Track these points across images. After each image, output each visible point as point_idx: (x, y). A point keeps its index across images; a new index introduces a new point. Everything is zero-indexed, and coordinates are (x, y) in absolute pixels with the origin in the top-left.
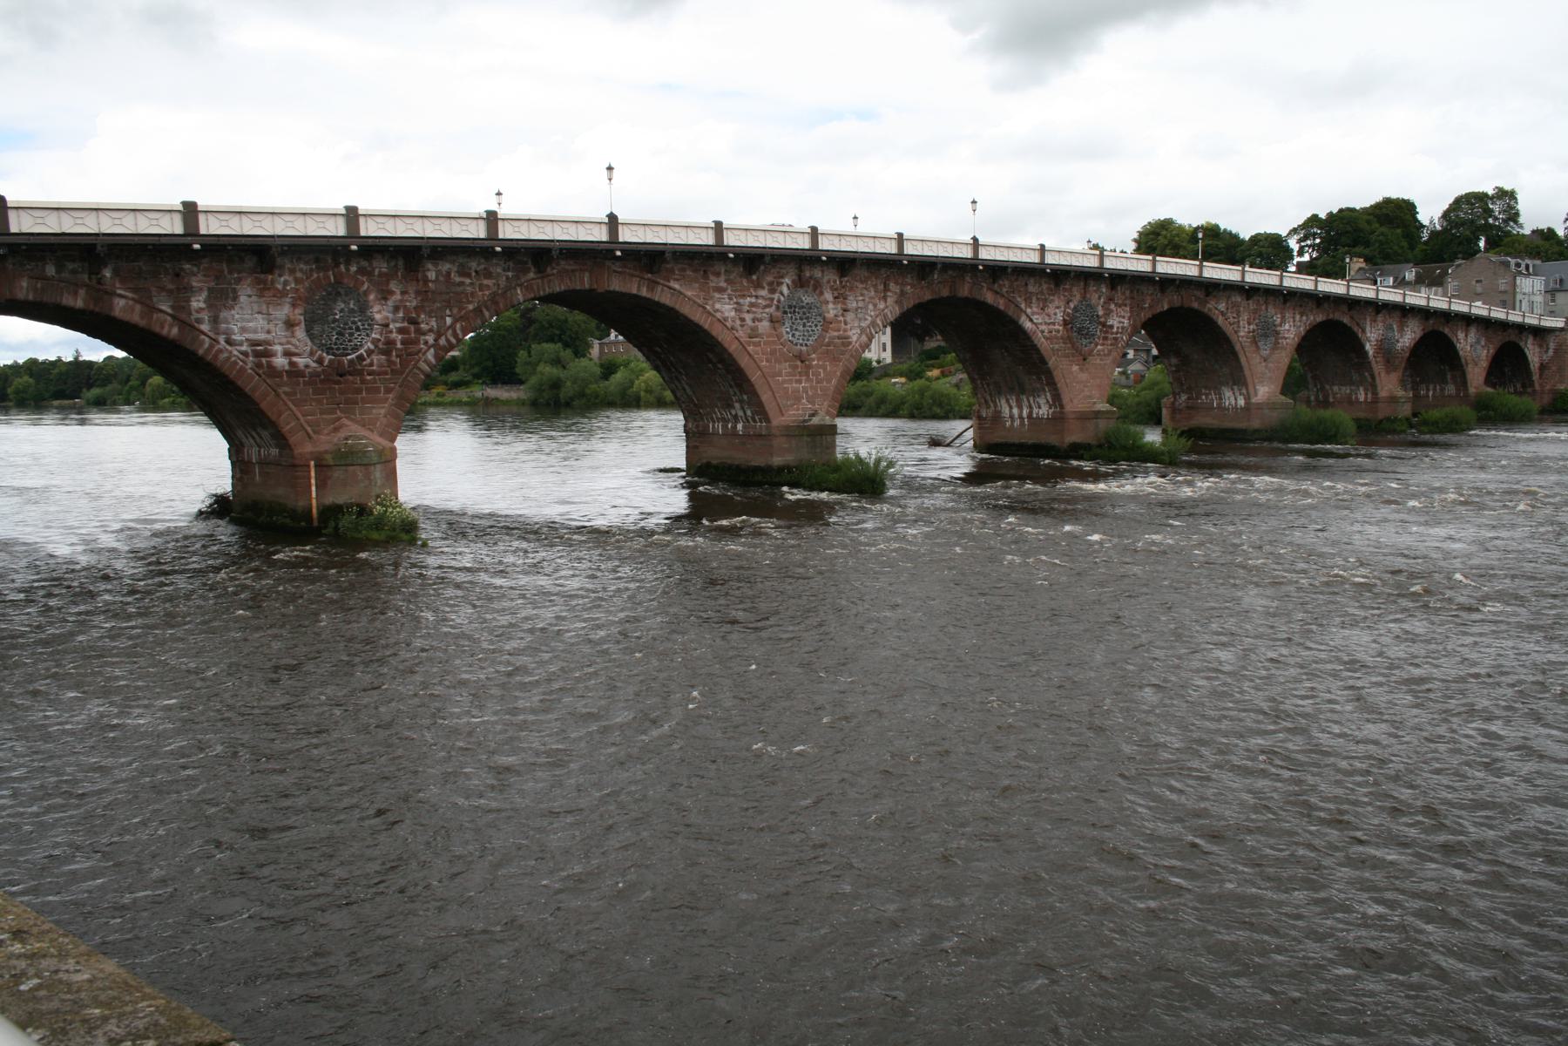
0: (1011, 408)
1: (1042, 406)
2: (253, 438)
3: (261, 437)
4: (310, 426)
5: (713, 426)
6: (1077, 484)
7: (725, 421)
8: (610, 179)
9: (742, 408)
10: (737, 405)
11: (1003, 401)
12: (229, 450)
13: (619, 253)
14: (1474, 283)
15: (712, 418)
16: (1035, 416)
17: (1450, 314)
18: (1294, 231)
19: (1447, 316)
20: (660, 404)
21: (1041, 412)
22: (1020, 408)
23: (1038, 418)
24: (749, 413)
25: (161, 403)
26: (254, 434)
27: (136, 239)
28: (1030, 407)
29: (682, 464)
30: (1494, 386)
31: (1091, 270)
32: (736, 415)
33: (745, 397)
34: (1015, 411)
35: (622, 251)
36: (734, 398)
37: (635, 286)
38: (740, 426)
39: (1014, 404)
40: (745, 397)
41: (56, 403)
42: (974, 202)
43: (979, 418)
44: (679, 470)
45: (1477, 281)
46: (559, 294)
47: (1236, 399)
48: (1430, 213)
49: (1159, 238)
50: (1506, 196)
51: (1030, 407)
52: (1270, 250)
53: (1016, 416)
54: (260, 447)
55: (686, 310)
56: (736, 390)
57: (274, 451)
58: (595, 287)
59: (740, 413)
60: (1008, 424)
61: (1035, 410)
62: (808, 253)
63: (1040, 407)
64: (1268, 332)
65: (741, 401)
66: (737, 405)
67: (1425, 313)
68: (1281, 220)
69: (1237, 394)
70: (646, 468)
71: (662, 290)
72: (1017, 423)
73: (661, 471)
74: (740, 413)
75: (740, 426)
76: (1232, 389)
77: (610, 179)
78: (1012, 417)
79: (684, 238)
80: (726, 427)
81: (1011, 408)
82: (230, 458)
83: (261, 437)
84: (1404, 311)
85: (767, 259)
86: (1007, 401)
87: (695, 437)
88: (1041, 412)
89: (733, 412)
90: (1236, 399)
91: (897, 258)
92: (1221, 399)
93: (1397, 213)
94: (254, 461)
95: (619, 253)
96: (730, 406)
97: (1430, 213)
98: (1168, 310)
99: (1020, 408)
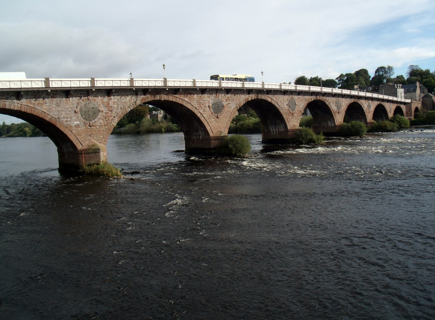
0: (273, 129)
1: (282, 128)
2: (65, 145)
3: (68, 146)
4: (82, 142)
5: (193, 138)
6: (269, 153)
7: (196, 136)
8: (164, 69)
9: (202, 132)
10: (200, 131)
11: (271, 127)
12: (58, 149)
13: (167, 89)
14: (386, 91)
15: (193, 135)
16: (280, 131)
17: (373, 98)
18: (337, 79)
19: (383, 100)
20: (169, 131)
21: (281, 130)
22: (275, 129)
23: (281, 131)
24: (203, 133)
25: (37, 135)
26: (65, 144)
27: (13, 89)
28: (278, 128)
29: (184, 149)
30: (375, 120)
31: (161, 88)
32: (200, 134)
33: (202, 129)
34: (274, 130)
35: (168, 89)
36: (199, 129)
37: (171, 98)
38: (201, 137)
39: (273, 128)
40: (202, 129)
41: (414, 126)
42: (262, 72)
43: (264, 132)
44: (182, 151)
45: (387, 91)
46: (151, 101)
47: (332, 124)
48: (372, 74)
49: (301, 81)
50: (390, 68)
51: (278, 128)
52: (330, 83)
53: (275, 131)
54: (67, 148)
55: (185, 104)
56: (200, 127)
57: (72, 149)
58: (160, 99)
59: (201, 133)
60: (272, 133)
61: (280, 130)
62: (163, 87)
63: (281, 129)
64: (292, 105)
65: (201, 130)
66: (200, 131)
67: (378, 99)
68: (334, 75)
69: (332, 123)
70: (169, 152)
71: (179, 99)
72: (275, 133)
73: (176, 151)
74: (201, 133)
75: (201, 137)
76: (331, 122)
77: (164, 69)
78: (273, 131)
79: (231, 85)
80: (196, 137)
81: (273, 129)
82: (58, 152)
83: (68, 146)
84: (372, 99)
85: (150, 90)
86: (272, 127)
87: (188, 140)
88: (281, 130)
89: (199, 133)
90: (332, 124)
91: (164, 87)
92: (327, 124)
93: (362, 73)
94: (65, 152)
95: (167, 89)
96: (198, 131)
97: (372, 74)
98: (313, 101)
99: (275, 129)
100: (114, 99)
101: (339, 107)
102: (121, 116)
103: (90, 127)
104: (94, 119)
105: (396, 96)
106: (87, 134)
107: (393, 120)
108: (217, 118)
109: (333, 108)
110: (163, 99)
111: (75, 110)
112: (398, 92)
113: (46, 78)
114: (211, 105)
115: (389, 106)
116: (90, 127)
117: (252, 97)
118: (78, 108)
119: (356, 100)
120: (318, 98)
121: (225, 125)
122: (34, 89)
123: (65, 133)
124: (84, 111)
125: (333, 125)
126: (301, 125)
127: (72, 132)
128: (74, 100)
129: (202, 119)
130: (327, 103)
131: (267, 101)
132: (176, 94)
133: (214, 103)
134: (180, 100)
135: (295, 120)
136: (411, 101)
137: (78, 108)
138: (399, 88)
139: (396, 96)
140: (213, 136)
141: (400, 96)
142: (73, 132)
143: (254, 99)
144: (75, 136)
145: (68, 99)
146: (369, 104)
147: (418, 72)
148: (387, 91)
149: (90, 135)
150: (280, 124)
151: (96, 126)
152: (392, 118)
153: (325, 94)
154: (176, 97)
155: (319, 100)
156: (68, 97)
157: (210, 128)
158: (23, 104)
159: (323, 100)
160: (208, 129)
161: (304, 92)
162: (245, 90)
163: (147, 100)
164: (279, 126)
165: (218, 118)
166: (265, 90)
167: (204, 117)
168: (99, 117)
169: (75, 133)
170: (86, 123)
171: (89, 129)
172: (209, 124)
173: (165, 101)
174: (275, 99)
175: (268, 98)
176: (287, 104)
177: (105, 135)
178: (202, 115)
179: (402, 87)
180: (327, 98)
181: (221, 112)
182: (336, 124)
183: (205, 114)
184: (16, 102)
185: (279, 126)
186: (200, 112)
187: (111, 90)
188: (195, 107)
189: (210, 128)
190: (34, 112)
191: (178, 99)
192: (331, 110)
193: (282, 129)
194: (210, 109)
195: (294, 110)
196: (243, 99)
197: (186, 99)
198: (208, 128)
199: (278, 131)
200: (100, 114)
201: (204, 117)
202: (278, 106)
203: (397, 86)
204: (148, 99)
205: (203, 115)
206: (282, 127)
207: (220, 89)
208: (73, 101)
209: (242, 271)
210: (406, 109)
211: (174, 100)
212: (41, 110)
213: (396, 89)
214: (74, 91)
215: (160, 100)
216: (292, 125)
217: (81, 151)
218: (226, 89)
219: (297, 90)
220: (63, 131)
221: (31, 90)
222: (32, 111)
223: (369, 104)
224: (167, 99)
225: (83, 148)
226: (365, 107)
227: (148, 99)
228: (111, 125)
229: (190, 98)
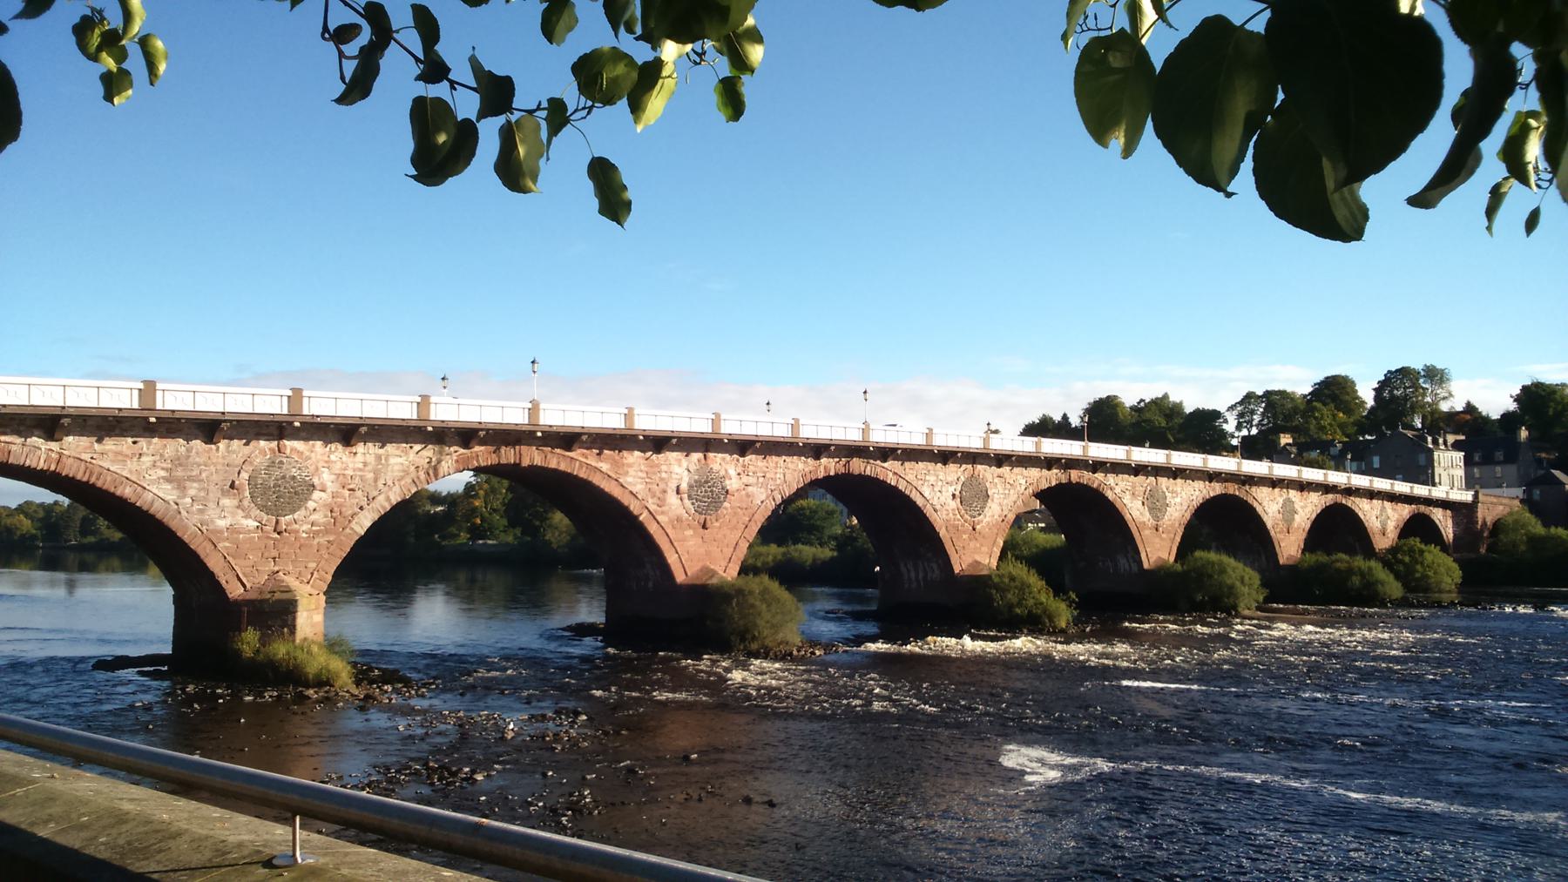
0: (909, 571)
1: (936, 570)
19: (1350, 491)
37: (555, 460)
47: (1130, 565)
53: (913, 579)
55: (597, 480)
58: (518, 462)
60: (906, 586)
61: (929, 575)
67: (1327, 488)
69: (1131, 561)
72: (914, 585)
75: (650, 585)
84: (1303, 486)
86: (906, 565)
100: (366, 452)
101: (1156, 504)
102: (383, 507)
103: (279, 533)
104: (293, 511)
105: (1430, 481)
106: (266, 555)
107: (1390, 559)
108: (704, 527)
109: (1136, 514)
110: (526, 463)
111: (233, 482)
112: (1436, 464)
113: (144, 382)
114: (684, 486)
115: (1376, 512)
116: (276, 536)
117: (829, 466)
118: (244, 475)
119: (1232, 489)
120: (1075, 475)
121: (728, 551)
122: (94, 410)
123: (192, 547)
124: (261, 484)
125: (1135, 568)
126: (745, 570)
127: (216, 546)
128: (231, 450)
129: (653, 528)
130: (1110, 495)
131: (884, 482)
132: (569, 449)
133: (696, 481)
134: (584, 469)
135: (982, 545)
136: (1476, 496)
137: (244, 475)
138: (1442, 447)
139: (1430, 481)
140: (686, 582)
141: (1445, 479)
142: (220, 546)
143: (837, 475)
144: (225, 558)
145: (213, 446)
146: (1288, 502)
147: (1544, 390)
148: (1396, 456)
149: (274, 558)
150: (930, 555)
151: (297, 531)
152: (1393, 550)
153: (1098, 466)
154: (572, 458)
155: (1078, 483)
156: (214, 440)
157: (680, 558)
158: (65, 452)
159: (1095, 486)
160: (669, 561)
161: (1019, 456)
162: (801, 444)
163: (475, 462)
164: (926, 564)
165: (707, 529)
166: (871, 449)
167: (658, 523)
168: (311, 505)
169: (226, 548)
170: (263, 523)
171: (275, 539)
172: (675, 544)
173: (532, 468)
174: (910, 477)
175: (888, 472)
176: (954, 496)
177: (323, 562)
178: (653, 515)
179: (1457, 446)
180: (1111, 479)
181: (717, 511)
182: (1146, 566)
183: (663, 513)
184: (43, 448)
185: (926, 564)
186: (647, 508)
187: (356, 427)
188: (631, 492)
189: (680, 558)
190: (98, 479)
191: (578, 463)
192: (1127, 517)
193: (936, 574)
194: (681, 499)
195: (980, 515)
196: (791, 473)
197: (604, 467)
198: (671, 559)
199: (925, 578)
200: (316, 495)
201: (658, 523)
202: (920, 502)
203: (1435, 442)
204: (478, 461)
205: (658, 518)
206: (935, 566)
207: (715, 439)
208: (228, 452)
209: (553, 679)
210: (1455, 524)
211: (563, 467)
212: (122, 476)
213: (1431, 452)
214: (234, 423)
215: (517, 466)
216: (970, 560)
217: (238, 604)
218: (737, 440)
219: (989, 451)
220: (187, 542)
221: (94, 412)
222: (91, 474)
223: (1288, 502)
224: (539, 464)
225: (247, 598)
226: (1270, 515)
227: (478, 461)
228: (348, 530)
229: (616, 464)
